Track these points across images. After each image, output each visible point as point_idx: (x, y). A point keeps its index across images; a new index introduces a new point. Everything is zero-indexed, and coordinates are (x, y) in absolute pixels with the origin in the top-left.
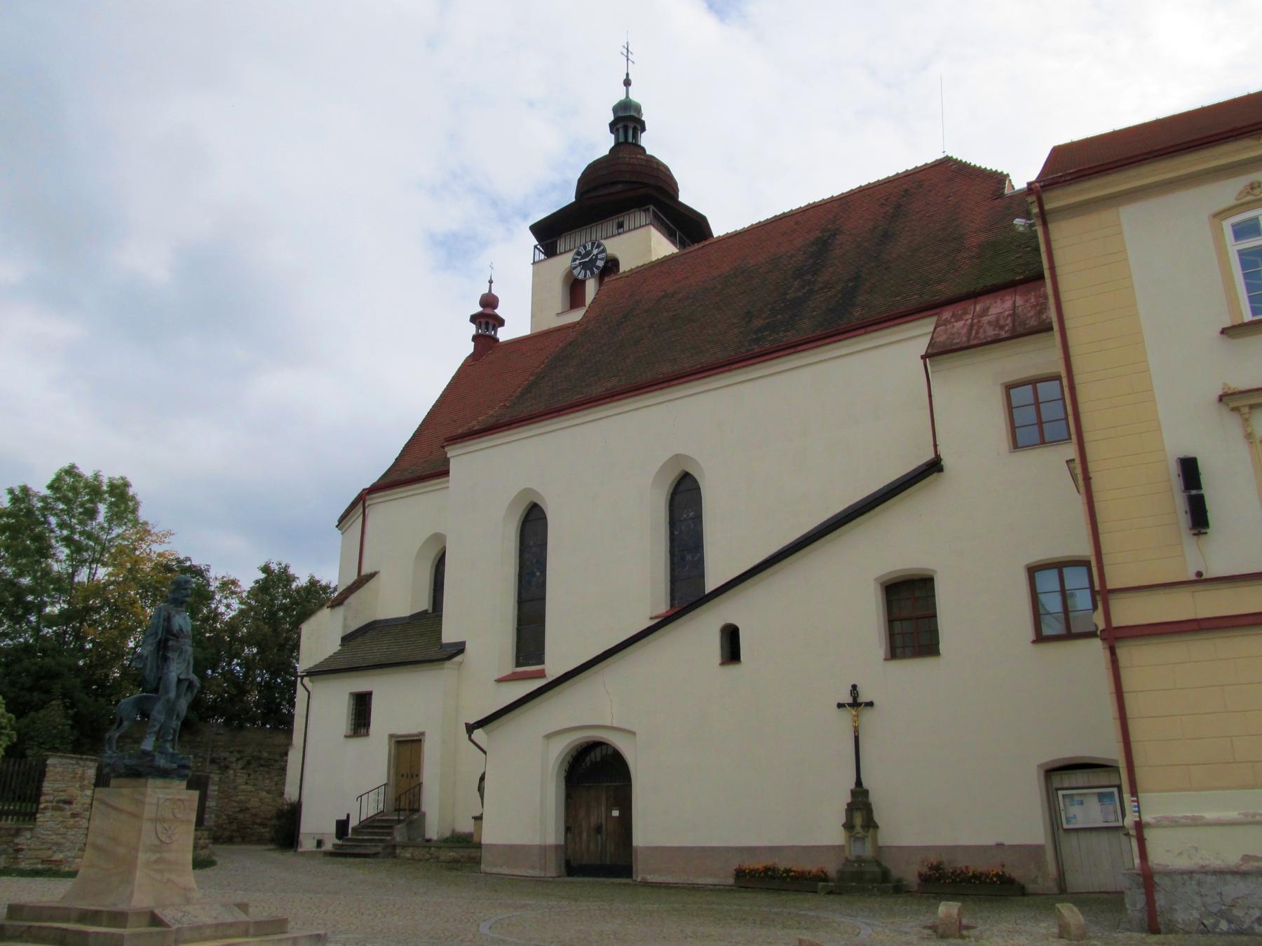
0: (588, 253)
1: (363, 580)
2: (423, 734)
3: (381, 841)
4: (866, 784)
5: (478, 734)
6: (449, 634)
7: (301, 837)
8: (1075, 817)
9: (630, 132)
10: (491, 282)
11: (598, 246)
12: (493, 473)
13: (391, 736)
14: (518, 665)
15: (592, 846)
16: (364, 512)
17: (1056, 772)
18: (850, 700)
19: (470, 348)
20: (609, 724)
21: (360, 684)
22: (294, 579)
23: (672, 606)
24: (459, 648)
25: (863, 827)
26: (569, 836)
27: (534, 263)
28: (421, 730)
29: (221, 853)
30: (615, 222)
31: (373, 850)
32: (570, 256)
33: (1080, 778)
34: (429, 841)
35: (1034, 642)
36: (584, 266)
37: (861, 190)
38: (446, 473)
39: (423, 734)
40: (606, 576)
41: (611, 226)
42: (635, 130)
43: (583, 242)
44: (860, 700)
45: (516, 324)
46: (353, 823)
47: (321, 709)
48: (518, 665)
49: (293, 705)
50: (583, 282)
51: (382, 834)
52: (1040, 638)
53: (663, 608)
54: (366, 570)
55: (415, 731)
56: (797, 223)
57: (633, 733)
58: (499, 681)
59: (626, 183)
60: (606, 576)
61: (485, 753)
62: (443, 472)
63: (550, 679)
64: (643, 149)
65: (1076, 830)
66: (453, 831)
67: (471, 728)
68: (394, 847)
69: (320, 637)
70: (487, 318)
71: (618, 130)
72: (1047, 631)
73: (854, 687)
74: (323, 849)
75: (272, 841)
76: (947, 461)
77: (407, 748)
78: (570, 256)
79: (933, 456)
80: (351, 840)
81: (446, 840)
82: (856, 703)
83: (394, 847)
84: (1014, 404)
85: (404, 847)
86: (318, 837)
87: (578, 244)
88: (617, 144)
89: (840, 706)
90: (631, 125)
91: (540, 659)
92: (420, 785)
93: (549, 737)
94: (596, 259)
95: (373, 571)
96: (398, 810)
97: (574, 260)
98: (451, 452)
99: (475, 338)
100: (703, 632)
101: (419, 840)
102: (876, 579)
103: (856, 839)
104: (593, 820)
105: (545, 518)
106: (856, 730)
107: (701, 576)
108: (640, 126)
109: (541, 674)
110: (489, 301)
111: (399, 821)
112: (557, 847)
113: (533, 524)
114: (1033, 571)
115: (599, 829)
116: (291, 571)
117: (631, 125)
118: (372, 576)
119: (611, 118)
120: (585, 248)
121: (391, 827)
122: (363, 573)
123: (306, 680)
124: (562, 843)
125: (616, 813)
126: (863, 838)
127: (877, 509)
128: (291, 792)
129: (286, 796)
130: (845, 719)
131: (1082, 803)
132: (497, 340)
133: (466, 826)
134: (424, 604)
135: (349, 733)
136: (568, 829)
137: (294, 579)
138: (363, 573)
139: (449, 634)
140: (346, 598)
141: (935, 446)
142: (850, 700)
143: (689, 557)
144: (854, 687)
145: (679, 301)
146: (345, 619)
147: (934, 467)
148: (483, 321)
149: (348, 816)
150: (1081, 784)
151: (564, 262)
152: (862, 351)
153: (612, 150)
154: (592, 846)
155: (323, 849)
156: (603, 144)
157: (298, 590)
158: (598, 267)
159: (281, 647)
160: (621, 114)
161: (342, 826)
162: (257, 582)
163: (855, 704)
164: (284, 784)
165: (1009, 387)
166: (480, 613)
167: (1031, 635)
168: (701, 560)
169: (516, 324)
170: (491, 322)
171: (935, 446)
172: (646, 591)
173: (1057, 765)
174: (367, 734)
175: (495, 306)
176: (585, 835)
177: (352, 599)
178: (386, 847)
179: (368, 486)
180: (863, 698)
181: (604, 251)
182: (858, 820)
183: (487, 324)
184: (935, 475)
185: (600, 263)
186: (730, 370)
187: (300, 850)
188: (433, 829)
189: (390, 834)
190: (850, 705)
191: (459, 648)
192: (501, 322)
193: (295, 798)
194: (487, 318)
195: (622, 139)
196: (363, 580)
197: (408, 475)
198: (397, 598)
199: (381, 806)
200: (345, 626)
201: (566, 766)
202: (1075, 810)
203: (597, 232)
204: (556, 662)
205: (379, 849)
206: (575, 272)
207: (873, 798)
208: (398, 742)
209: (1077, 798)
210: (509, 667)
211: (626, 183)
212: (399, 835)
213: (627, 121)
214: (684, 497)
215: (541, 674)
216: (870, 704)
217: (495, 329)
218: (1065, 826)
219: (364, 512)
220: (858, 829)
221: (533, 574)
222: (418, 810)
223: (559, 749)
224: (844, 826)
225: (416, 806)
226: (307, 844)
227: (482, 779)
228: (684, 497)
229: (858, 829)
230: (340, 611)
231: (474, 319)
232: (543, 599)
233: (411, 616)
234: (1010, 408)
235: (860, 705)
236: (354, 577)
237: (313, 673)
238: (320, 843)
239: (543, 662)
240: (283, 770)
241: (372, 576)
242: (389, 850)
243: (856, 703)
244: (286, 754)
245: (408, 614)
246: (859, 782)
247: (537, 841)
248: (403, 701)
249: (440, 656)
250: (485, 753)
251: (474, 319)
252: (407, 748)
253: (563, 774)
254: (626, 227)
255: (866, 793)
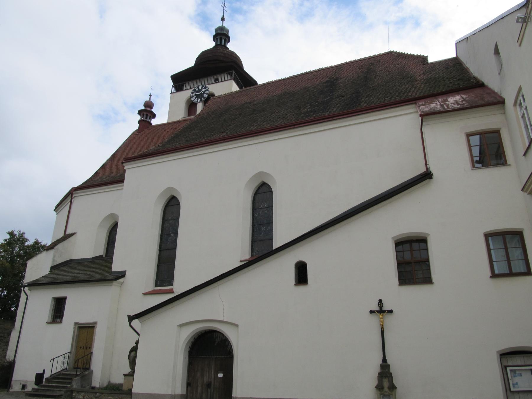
0: (200, 91)
1: (66, 237)
2: (96, 323)
3: (64, 387)
4: (389, 361)
5: (136, 323)
6: (116, 267)
7: (13, 383)
8: (517, 384)
9: (223, 41)
10: (150, 96)
11: (205, 88)
12: (150, 180)
13: (76, 324)
14: (156, 285)
15: (204, 396)
16: (71, 201)
17: (506, 355)
18: (378, 309)
19: (136, 127)
20: (221, 319)
21: (59, 292)
22: (27, 240)
23: (252, 255)
24: (122, 275)
25: (389, 388)
26: (189, 388)
27: (172, 93)
28: (94, 321)
29: (508, 164)
30: (215, 77)
31: (58, 393)
32: (191, 91)
33: (518, 360)
34: (94, 388)
35: (491, 277)
36: (197, 96)
37: (347, 63)
38: (122, 181)
39: (96, 323)
40: (213, 236)
41: (212, 79)
42: (225, 40)
43: (198, 85)
44: (384, 309)
45: (161, 118)
46: (47, 375)
47: (35, 307)
48: (156, 285)
49: (17, 307)
50: (196, 104)
51: (65, 383)
52: (494, 276)
53: (247, 256)
54: (69, 232)
55: (91, 321)
56: (315, 75)
57: (237, 326)
58: (145, 294)
59: (219, 61)
60: (213, 236)
61: (139, 335)
62: (120, 180)
63: (176, 294)
64: (228, 49)
65: (518, 392)
66: (109, 382)
67: (131, 319)
68: (72, 391)
69: (38, 268)
70: (147, 112)
71: (217, 39)
72: (497, 272)
73: (380, 301)
74: (26, 390)
75: (504, 109)
76: (433, 170)
77: (85, 332)
78: (191, 91)
79: (425, 170)
80: (44, 386)
81: (106, 388)
82: (381, 310)
83: (72, 391)
84: (472, 145)
85: (78, 392)
86: (24, 383)
87: (195, 86)
88: (216, 45)
89: (372, 312)
90: (224, 37)
91: (170, 282)
92: (91, 353)
93: (181, 326)
94: (204, 93)
95: (73, 232)
96: (76, 368)
97: (192, 93)
98: (127, 166)
99: (140, 122)
100: (283, 267)
101: (88, 387)
102: (393, 238)
103: (384, 396)
104: (206, 379)
105: (179, 204)
106: (382, 327)
107: (272, 239)
108: (228, 39)
109: (171, 291)
110: (149, 105)
111: (76, 375)
112: (182, 396)
113: (172, 207)
114: (487, 236)
115: (209, 385)
116: (26, 236)
117: (224, 37)
118: (72, 234)
119: (214, 34)
120: (198, 88)
121: (71, 379)
122: (67, 233)
123: (26, 289)
124: (185, 393)
125: (221, 375)
126: (389, 395)
127: (393, 198)
128: (10, 355)
129: (7, 358)
130: (374, 321)
131: (521, 375)
132: (151, 124)
133: (118, 379)
134: (101, 251)
135: (50, 321)
136: (189, 384)
137: (27, 240)
138: (67, 233)
139: (116, 267)
140: (56, 245)
141: (426, 165)
142: (378, 309)
143: (263, 229)
144: (380, 301)
145: (254, 105)
146: (54, 257)
147: (427, 176)
148: (145, 113)
149: (44, 371)
150: (519, 364)
151: (186, 94)
152: (364, 122)
153: (214, 47)
154: (204, 396)
155: (26, 390)
156: (208, 43)
157: (28, 246)
158: (204, 98)
159: (16, 275)
160: (219, 32)
161: (39, 377)
162: (6, 240)
163: (381, 311)
164: (7, 351)
165: (469, 135)
166: (136, 256)
167: (489, 274)
168: (271, 230)
169: (161, 118)
170: (149, 115)
171: (426, 165)
172: (237, 245)
173: (506, 351)
174: (61, 322)
175: (152, 108)
176: (200, 388)
177: (59, 246)
178: (67, 392)
179: (76, 186)
180: (386, 308)
181: (208, 90)
182: (386, 384)
183: (147, 115)
184: (428, 180)
185: (206, 96)
186: (294, 128)
187: (11, 390)
188: (97, 380)
189: (70, 383)
190: (378, 312)
191: (122, 275)
192: (154, 116)
193: (12, 358)
194: (147, 112)
195: (219, 43)
196: (66, 237)
197: (97, 183)
198: (86, 246)
199: (65, 366)
200: (54, 260)
201: (190, 345)
202: (517, 379)
203: (205, 82)
204: (180, 285)
205: (62, 393)
206: (192, 99)
207: (392, 370)
208: (80, 328)
209: (517, 372)
210: (151, 286)
211: (219, 61)
212: (75, 384)
213: (222, 36)
214: (262, 198)
215: (171, 291)
216: (391, 312)
217: (150, 118)
218: (512, 389)
219: (71, 201)
220: (386, 389)
221: (169, 235)
222: (89, 369)
223: (188, 333)
224: (376, 387)
225: (88, 366)
226: (16, 387)
227: (134, 350)
228: (262, 198)
229: (386, 389)
230: (51, 252)
231: (140, 112)
232: (175, 249)
233: (93, 258)
234: (470, 147)
235: (384, 311)
236: (62, 235)
237: (31, 285)
238: (24, 387)
239: (172, 285)
240: (8, 342)
241: (72, 234)
242: (69, 393)
243: (381, 310)
244: (10, 334)
245: (91, 256)
246: (384, 360)
247: (170, 392)
248: (85, 303)
249: (111, 278)
250: (139, 335)
251: (140, 112)
252: (85, 332)
253: (188, 350)
254: (220, 80)
255: (388, 366)
